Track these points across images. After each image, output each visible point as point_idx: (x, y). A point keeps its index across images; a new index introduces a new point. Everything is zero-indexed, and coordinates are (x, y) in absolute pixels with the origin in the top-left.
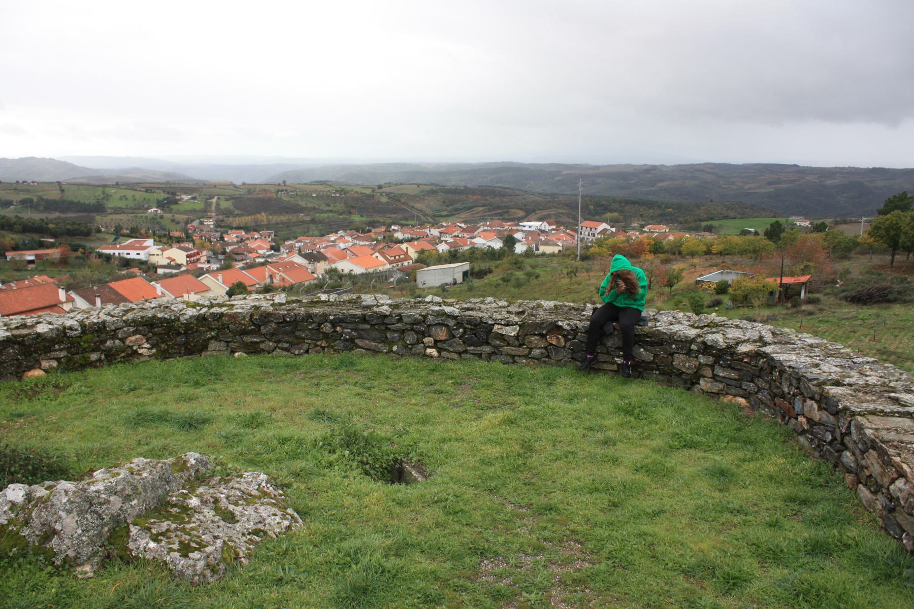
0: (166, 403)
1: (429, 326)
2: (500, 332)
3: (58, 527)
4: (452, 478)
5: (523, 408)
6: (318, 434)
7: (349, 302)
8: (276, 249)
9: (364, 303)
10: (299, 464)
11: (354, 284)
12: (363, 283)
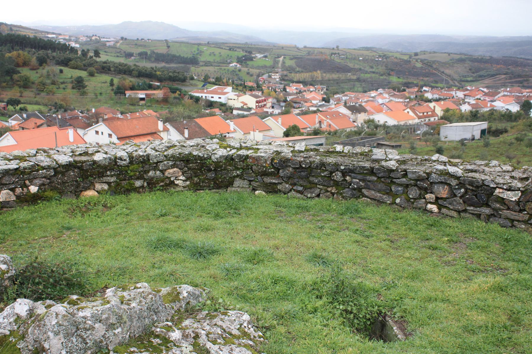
0: (186, 231)
1: (431, 183)
2: (501, 195)
3: (46, 346)
4: (430, 343)
5: (515, 275)
6: (309, 278)
7: (361, 154)
8: (326, 100)
9: (374, 157)
10: (286, 306)
11: (387, 133)
12: (394, 133)
